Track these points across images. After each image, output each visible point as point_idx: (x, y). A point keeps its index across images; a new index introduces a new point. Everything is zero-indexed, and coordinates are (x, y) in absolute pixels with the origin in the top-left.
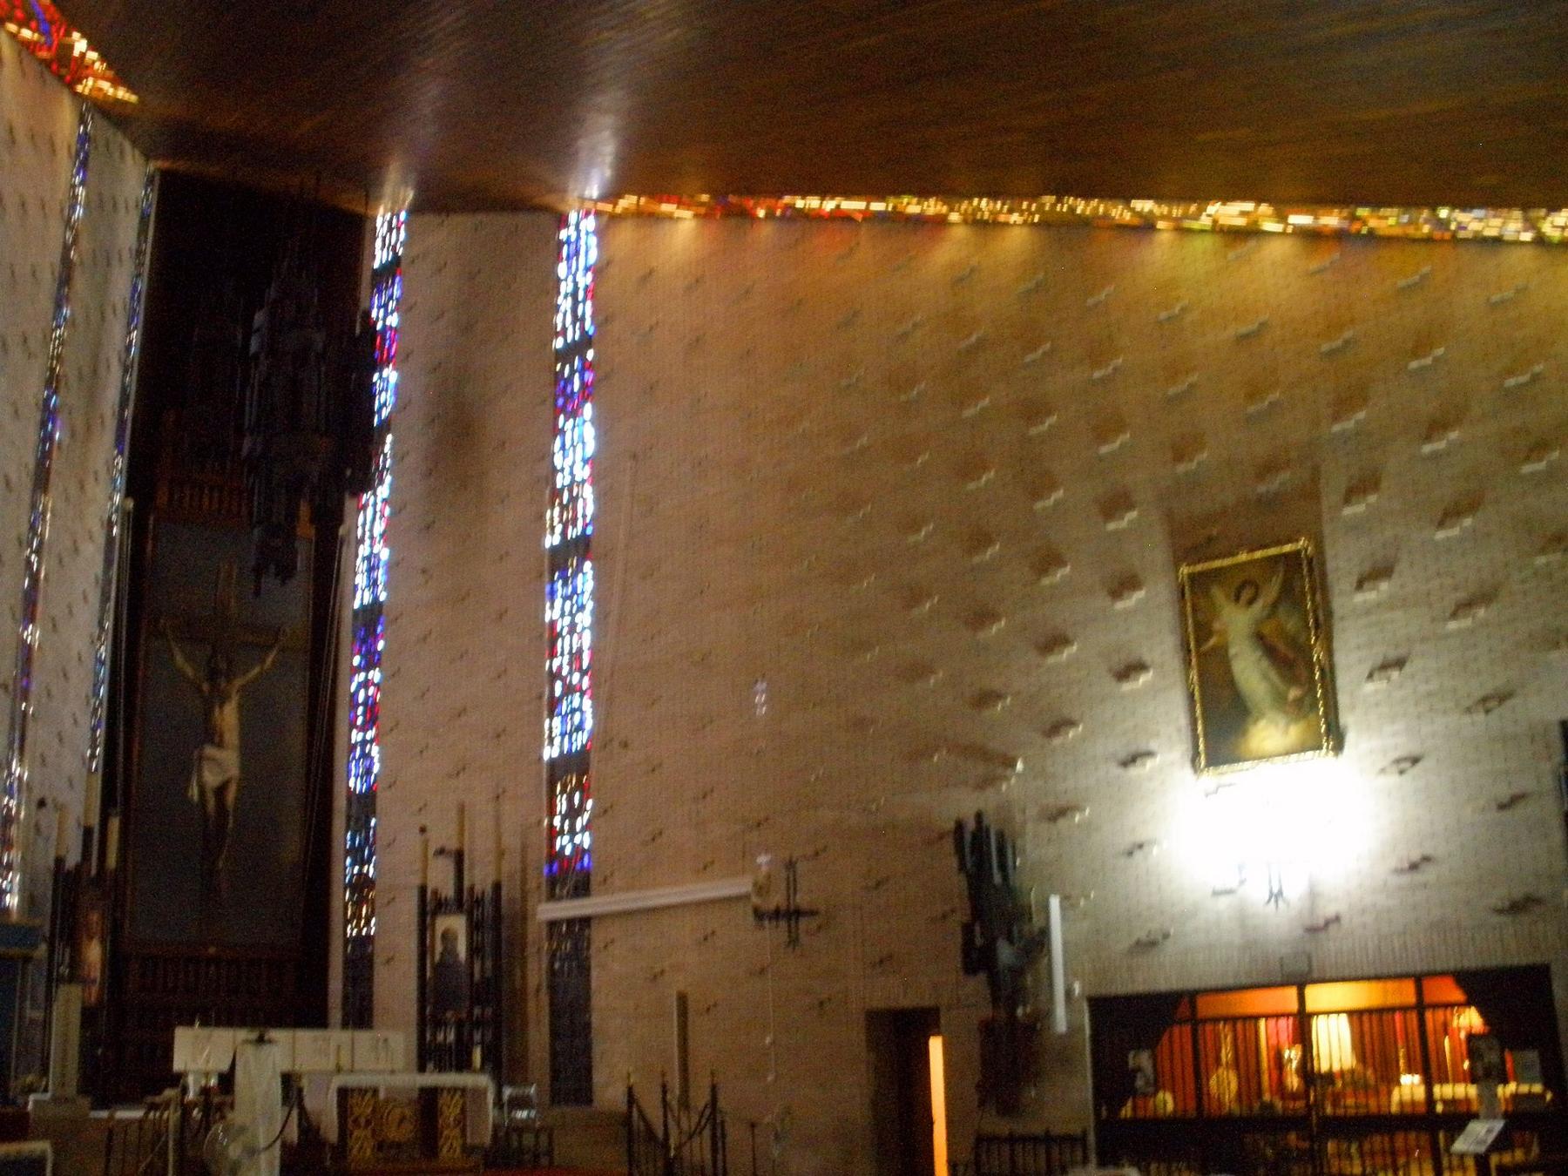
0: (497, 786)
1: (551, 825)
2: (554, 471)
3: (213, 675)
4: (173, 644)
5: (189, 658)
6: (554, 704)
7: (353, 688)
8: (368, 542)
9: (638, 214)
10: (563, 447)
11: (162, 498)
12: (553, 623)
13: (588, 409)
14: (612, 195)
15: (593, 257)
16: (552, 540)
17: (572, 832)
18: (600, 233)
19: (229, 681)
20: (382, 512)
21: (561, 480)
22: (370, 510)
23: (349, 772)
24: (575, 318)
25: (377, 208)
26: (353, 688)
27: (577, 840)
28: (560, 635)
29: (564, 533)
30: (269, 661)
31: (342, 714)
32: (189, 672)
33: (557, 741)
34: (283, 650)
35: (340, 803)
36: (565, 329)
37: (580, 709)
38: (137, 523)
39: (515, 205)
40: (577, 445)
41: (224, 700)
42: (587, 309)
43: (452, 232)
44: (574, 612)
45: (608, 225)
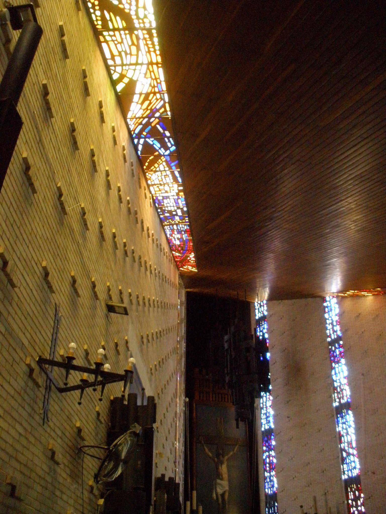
0: (325, 489)
1: (348, 503)
2: (333, 381)
3: (218, 455)
4: (204, 445)
5: (210, 450)
6: (343, 459)
7: (264, 457)
8: (265, 409)
9: (352, 296)
10: (336, 374)
11: (197, 397)
12: (339, 432)
13: (343, 361)
14: (344, 290)
15: (337, 311)
16: (336, 404)
17: (357, 506)
18: (339, 303)
19: (223, 457)
20: (269, 398)
21: (336, 384)
22: (264, 398)
23: (265, 486)
24: (334, 331)
25: (255, 300)
26: (264, 457)
27: (359, 508)
28: (343, 436)
29: (340, 402)
30: (236, 449)
31: (261, 467)
32: (210, 454)
33: (346, 472)
34: (239, 445)
35: (263, 498)
36: (330, 335)
37: (354, 462)
38: (189, 406)
39: (313, 296)
40: (341, 373)
41: (222, 463)
42: (337, 328)
43: (283, 306)
44: (348, 427)
45: (341, 300)
